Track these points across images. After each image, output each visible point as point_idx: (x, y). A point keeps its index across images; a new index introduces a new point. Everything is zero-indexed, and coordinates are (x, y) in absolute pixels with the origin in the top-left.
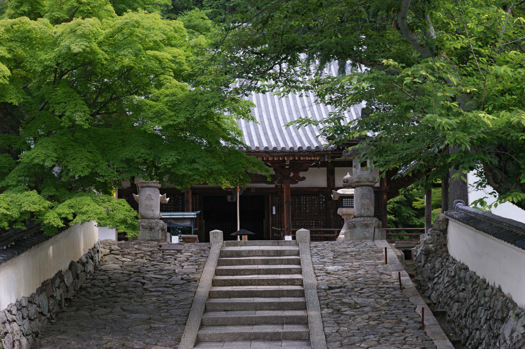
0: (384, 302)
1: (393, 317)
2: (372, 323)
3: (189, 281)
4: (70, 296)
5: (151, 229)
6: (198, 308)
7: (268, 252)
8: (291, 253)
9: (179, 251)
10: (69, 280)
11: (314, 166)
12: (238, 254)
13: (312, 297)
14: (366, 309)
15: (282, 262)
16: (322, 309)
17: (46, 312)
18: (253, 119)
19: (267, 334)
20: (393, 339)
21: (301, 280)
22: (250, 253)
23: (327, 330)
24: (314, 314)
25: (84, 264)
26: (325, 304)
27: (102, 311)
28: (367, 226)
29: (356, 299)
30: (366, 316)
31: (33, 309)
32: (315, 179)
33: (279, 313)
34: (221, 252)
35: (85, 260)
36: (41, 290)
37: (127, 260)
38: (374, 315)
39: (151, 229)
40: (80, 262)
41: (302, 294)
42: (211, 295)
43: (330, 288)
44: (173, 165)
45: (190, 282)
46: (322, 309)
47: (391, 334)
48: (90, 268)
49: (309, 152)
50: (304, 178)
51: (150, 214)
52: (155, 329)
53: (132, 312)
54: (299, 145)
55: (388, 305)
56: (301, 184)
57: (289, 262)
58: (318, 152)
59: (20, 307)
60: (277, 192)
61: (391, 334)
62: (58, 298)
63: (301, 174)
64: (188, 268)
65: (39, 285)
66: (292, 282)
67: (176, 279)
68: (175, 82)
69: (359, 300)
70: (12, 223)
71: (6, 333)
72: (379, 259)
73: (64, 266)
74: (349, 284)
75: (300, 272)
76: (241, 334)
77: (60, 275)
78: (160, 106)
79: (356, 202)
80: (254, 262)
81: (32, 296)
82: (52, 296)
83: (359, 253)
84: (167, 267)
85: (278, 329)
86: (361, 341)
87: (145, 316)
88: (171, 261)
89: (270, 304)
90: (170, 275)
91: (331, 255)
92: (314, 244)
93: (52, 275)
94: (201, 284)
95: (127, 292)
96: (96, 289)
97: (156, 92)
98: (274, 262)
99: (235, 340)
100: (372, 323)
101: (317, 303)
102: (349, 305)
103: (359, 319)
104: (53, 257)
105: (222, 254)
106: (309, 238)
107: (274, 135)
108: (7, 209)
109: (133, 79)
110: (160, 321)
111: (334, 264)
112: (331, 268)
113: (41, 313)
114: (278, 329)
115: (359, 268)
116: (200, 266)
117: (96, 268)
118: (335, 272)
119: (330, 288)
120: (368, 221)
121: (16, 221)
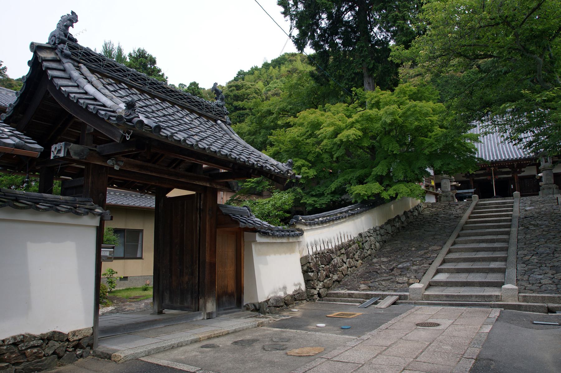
0: (553, 223)
1: (557, 230)
2: (544, 233)
3: (458, 217)
4: (404, 225)
5: (447, 196)
6: (458, 229)
7: (499, 203)
8: (510, 203)
9: (457, 205)
10: (403, 219)
11: (529, 166)
12: (485, 204)
13: (515, 222)
14: (543, 227)
15: (504, 207)
16: (519, 227)
17: (390, 232)
18: (481, 142)
19: (488, 239)
20: (554, 240)
21: (512, 214)
22: (490, 204)
23: (519, 237)
24: (514, 230)
25: (412, 212)
26: (521, 224)
27: (416, 231)
28: (550, 188)
29: (538, 222)
30: (542, 230)
31: (382, 231)
32: (529, 171)
33: (497, 230)
34: (476, 204)
35: (412, 210)
36: (387, 223)
37: (434, 210)
38: (546, 229)
39: (447, 196)
40: (410, 211)
41: (510, 220)
42: (467, 223)
43: (526, 217)
44: (440, 167)
45: (459, 217)
46: (519, 227)
47: (554, 238)
48: (416, 213)
49: (525, 159)
50: (524, 171)
51: (446, 190)
52: (436, 238)
53: (428, 231)
54: (519, 156)
55: (555, 224)
56: (522, 174)
57: (508, 207)
58: (529, 159)
59: (375, 230)
60: (512, 179)
61: (554, 238)
62: (398, 226)
63: (523, 169)
64: (459, 211)
65: (386, 221)
66: (507, 215)
67: (452, 217)
68: (439, 129)
69: (540, 223)
70: (368, 197)
71: (366, 241)
72: (554, 203)
73: (401, 213)
74: (536, 215)
75: (512, 211)
76: (475, 240)
77: (398, 217)
78: (431, 140)
79: (543, 179)
80: (491, 208)
81: (382, 226)
82: (394, 226)
83: (544, 201)
84: (450, 212)
85: (494, 237)
86: (536, 242)
87: (433, 233)
88: (453, 209)
89: (494, 226)
90: (450, 215)
91: (529, 202)
92: (522, 198)
93: (394, 217)
94: (463, 218)
95: (429, 223)
96: (416, 222)
97: (430, 134)
98: (501, 207)
99: (473, 243)
100: (544, 233)
101: (517, 224)
102: (534, 225)
103: (537, 231)
104: (393, 210)
105: (477, 205)
106: (519, 196)
107: (504, 154)
108: (366, 191)
109: (423, 130)
110: (440, 235)
111: (530, 206)
112: (528, 208)
113: (388, 233)
114: (494, 237)
115: (543, 207)
116: (464, 210)
117: (419, 213)
118: (530, 210)
119: (526, 217)
120: (551, 186)
121: (370, 196)
